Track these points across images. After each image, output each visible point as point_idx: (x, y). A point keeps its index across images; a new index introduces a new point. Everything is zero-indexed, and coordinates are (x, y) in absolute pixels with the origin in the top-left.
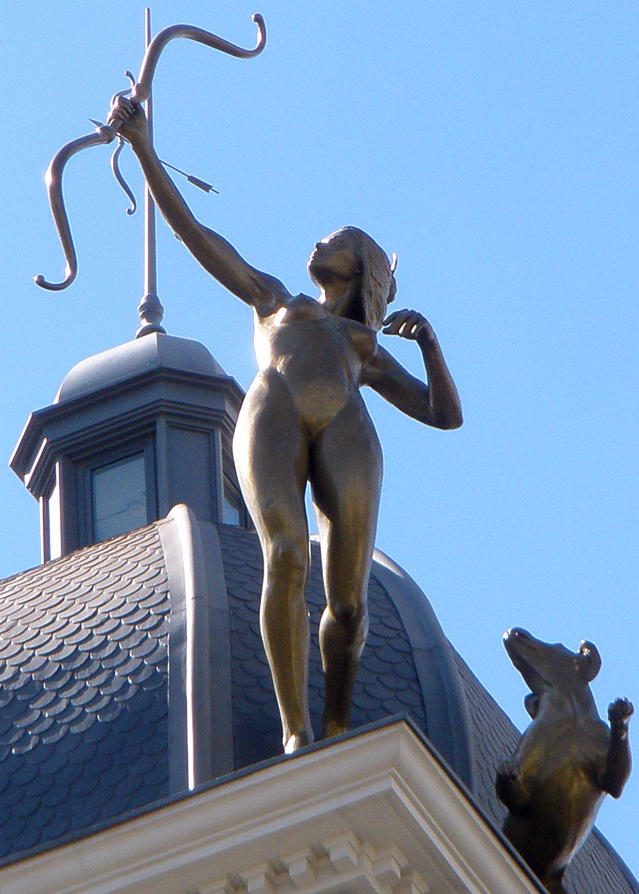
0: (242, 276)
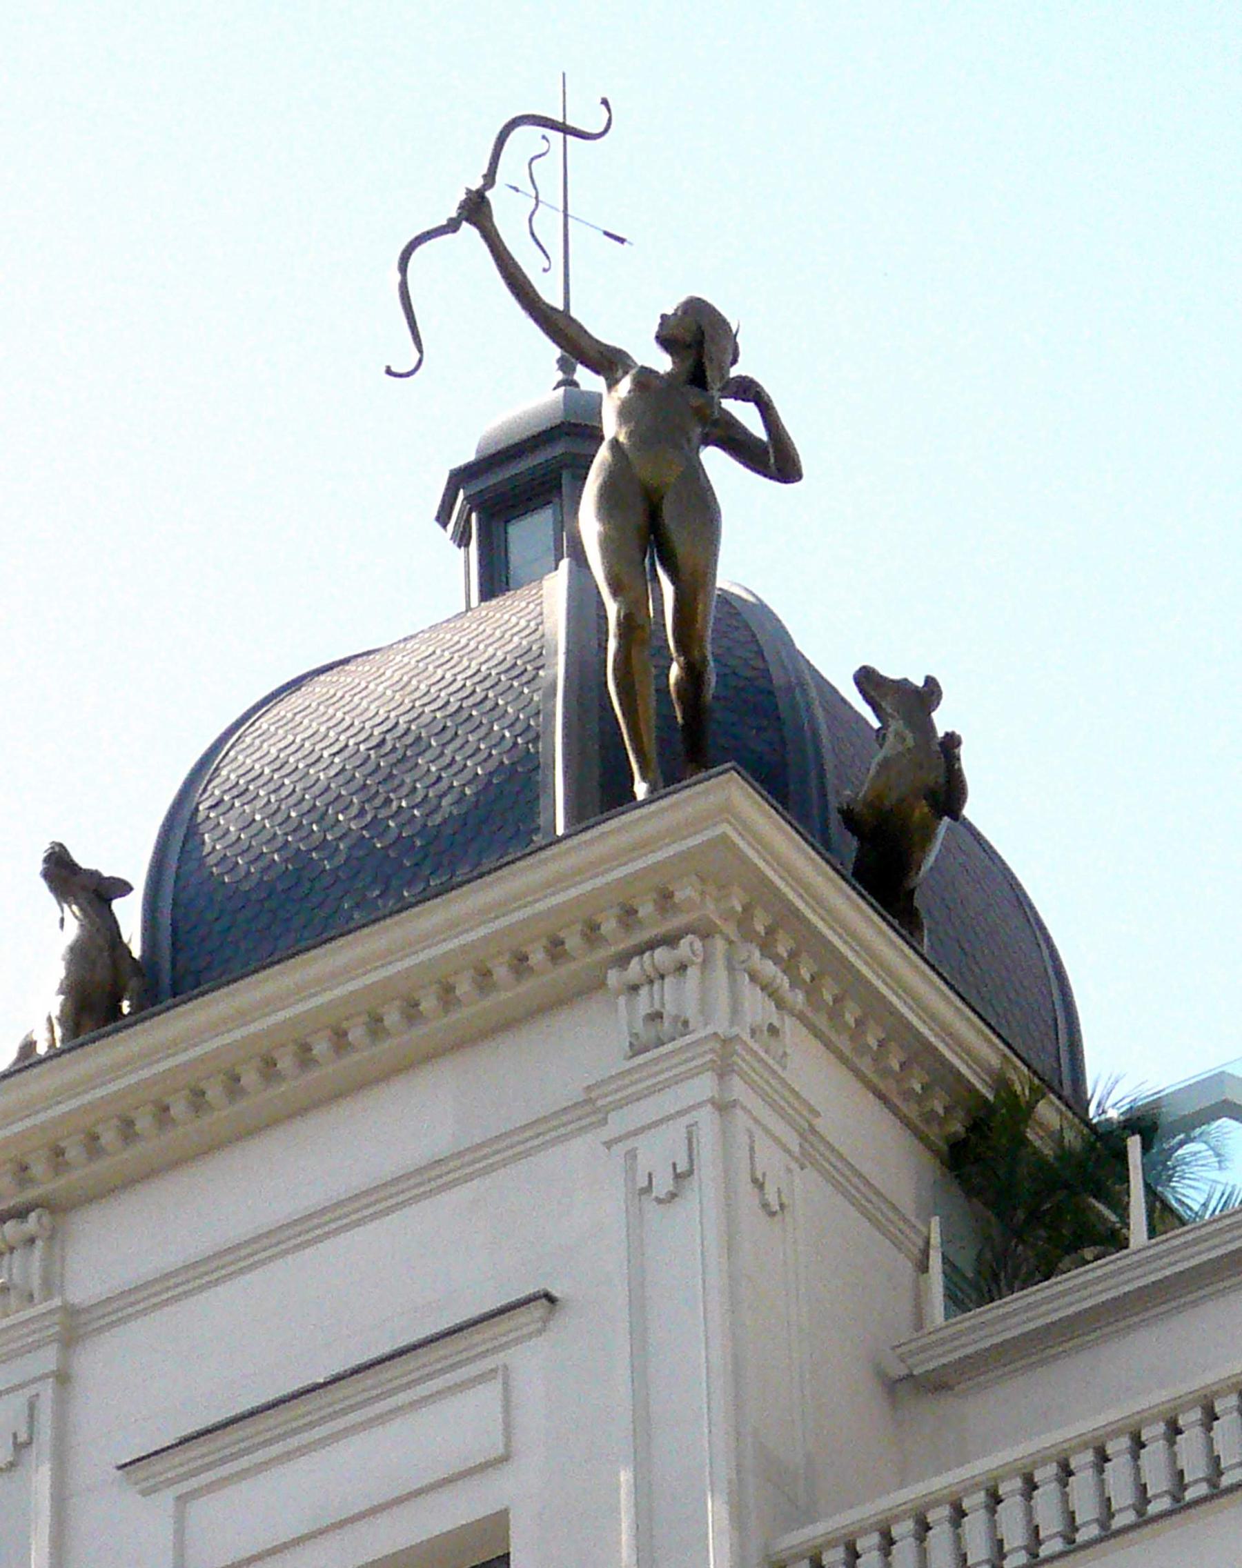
0: (592, 354)
